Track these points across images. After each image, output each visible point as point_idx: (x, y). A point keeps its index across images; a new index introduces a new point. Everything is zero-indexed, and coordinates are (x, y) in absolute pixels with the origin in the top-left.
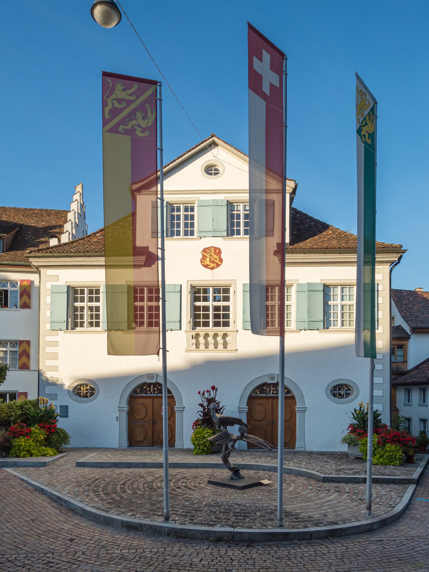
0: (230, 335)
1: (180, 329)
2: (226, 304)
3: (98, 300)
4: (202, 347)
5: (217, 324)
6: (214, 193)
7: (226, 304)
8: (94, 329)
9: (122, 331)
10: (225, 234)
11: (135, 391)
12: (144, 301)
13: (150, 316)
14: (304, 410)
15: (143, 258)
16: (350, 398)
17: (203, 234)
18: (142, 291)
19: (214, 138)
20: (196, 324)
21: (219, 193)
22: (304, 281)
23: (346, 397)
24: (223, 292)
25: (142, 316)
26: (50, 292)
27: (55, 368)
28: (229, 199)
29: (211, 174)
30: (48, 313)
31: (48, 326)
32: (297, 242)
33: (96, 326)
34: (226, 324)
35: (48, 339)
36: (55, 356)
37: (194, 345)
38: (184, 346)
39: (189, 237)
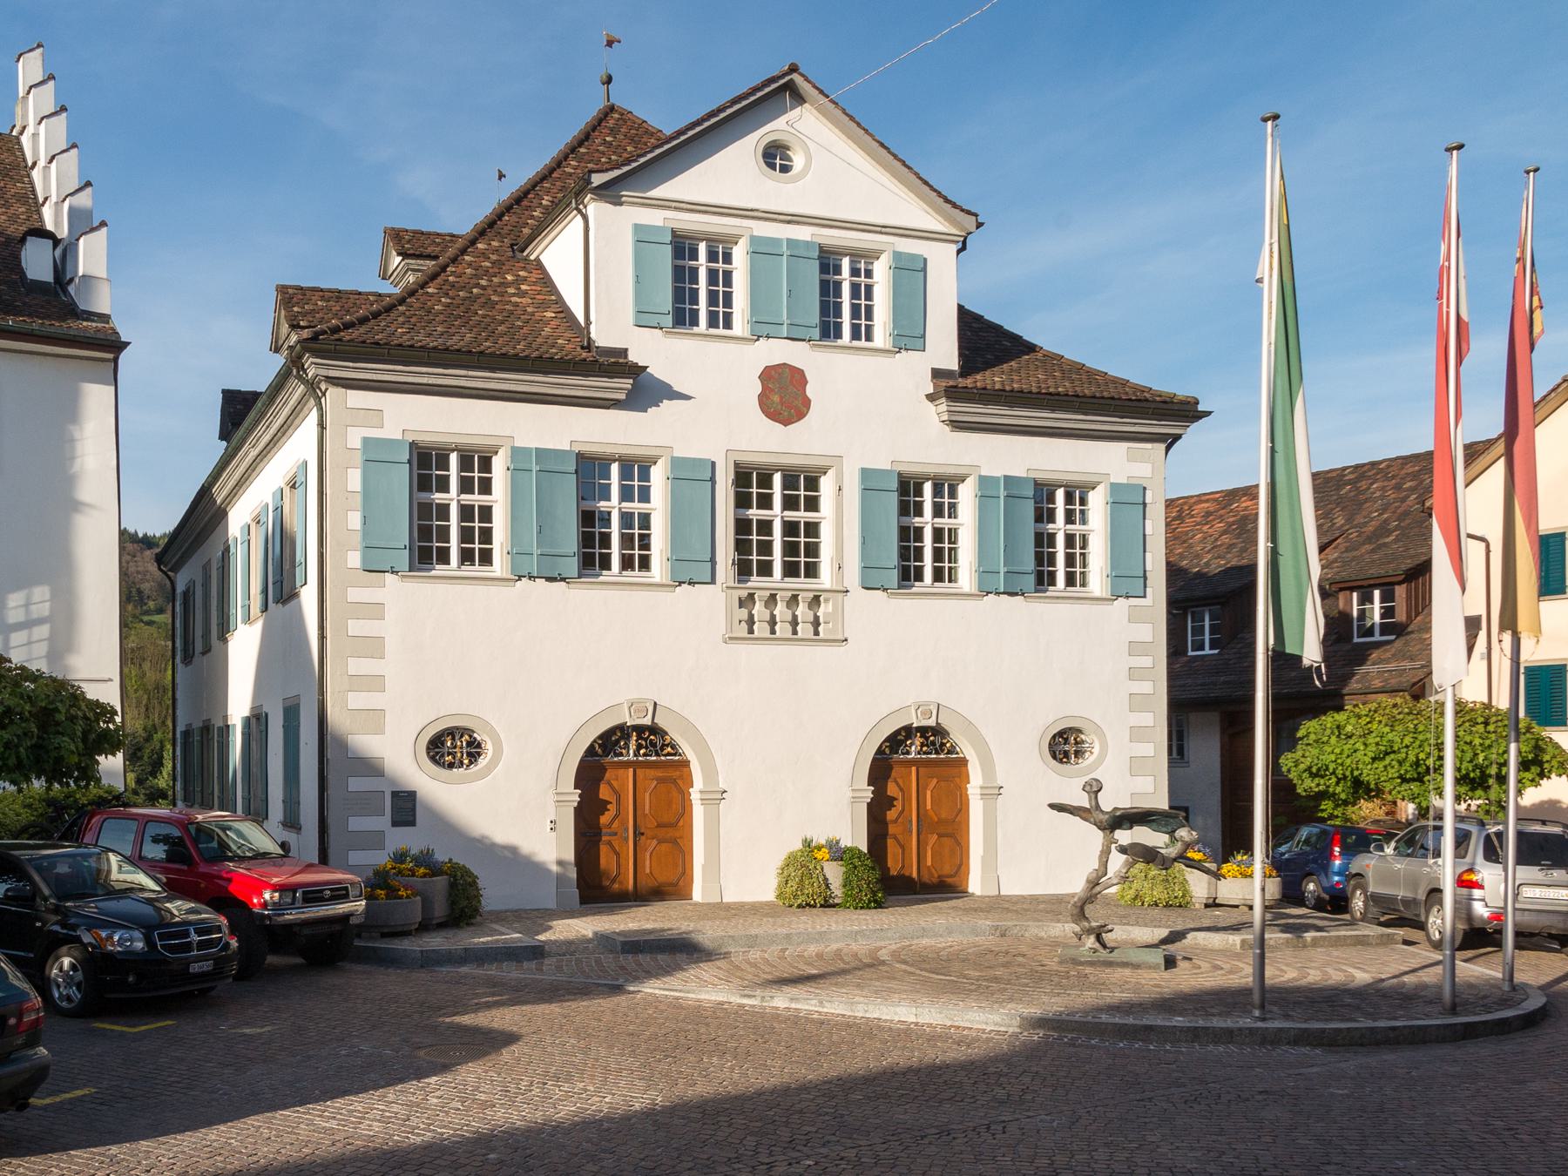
0: (827, 600)
1: (713, 582)
2: (811, 516)
3: (486, 487)
4: (761, 629)
5: (791, 570)
6: (789, 222)
7: (811, 516)
8: (477, 570)
9: (563, 579)
10: (816, 333)
11: (590, 751)
12: (447, 491)
13: (790, 549)
14: (716, 797)
15: (627, 383)
16: (483, 762)
17: (765, 329)
18: (766, 481)
19: (795, 76)
20: (743, 570)
21: (798, 223)
22: (997, 471)
23: (471, 763)
24: (803, 484)
25: (766, 548)
26: (358, 458)
27: (376, 683)
28: (677, 225)
29: (772, 166)
30: (355, 520)
31: (355, 559)
32: (977, 371)
33: (807, 576)
34: (812, 571)
35: (355, 595)
36: (374, 647)
37: (744, 626)
38: (720, 627)
39: (721, 331)
